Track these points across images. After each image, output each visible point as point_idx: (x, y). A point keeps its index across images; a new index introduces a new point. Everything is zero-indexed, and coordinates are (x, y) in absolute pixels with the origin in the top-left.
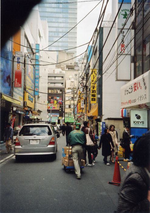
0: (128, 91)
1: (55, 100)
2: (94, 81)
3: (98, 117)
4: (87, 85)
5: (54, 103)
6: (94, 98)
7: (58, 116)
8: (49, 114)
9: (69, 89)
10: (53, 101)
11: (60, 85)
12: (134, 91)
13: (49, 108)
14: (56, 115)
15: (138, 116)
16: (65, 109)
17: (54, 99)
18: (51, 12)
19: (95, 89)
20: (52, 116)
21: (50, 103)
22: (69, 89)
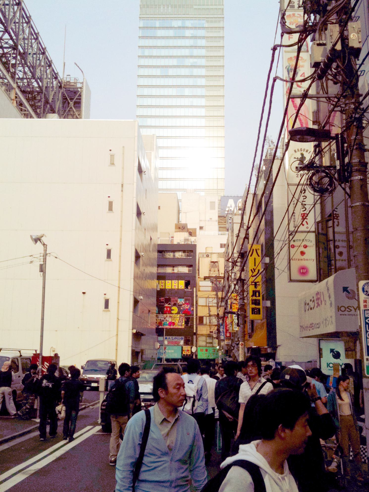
0: (308, 304)
1: (175, 305)
2: (257, 271)
3: (269, 350)
4: (243, 277)
5: (172, 312)
6: (257, 307)
7: (182, 342)
8: (161, 338)
9: (205, 278)
10: (170, 308)
11: (184, 270)
12: (317, 307)
13: (160, 323)
14: (176, 340)
15: (337, 352)
16: (198, 307)
17: (173, 303)
18: (163, 47)
19: (259, 288)
20: (169, 342)
21: (162, 313)
22: (205, 278)
